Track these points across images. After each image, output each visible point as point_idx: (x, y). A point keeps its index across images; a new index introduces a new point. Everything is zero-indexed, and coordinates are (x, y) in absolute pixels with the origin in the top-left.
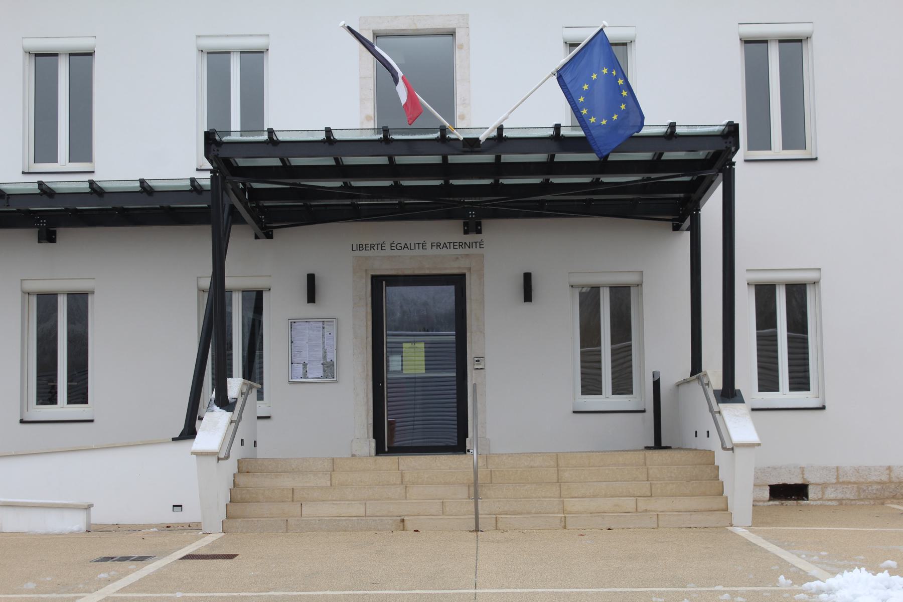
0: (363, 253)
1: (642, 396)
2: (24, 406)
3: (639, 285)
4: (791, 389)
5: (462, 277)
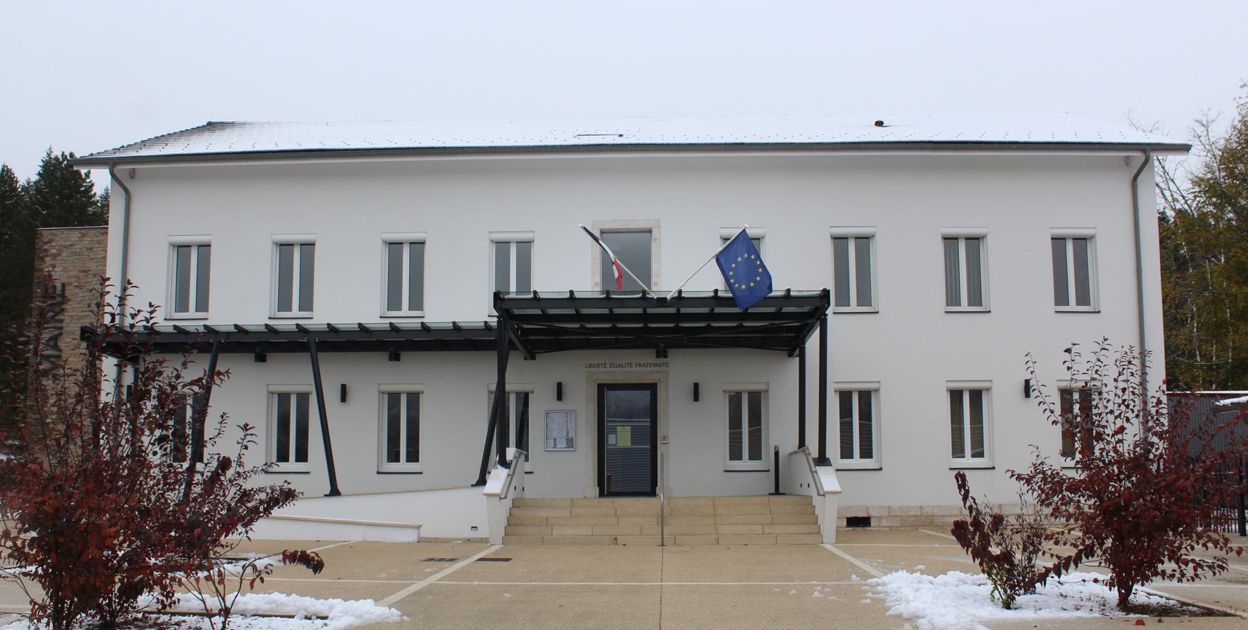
1: (767, 461)
3: (766, 391)
5: (655, 385)
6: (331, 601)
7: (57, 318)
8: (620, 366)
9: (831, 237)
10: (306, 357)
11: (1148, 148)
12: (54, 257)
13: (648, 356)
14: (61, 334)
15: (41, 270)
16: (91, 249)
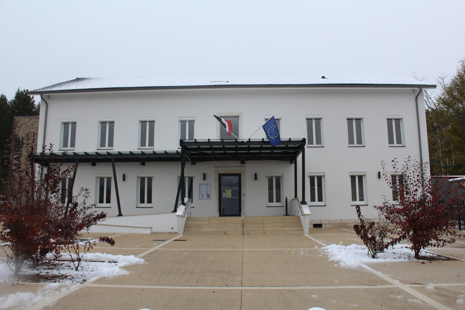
1: (283, 203)
2: (137, 204)
3: (282, 176)
6: (118, 256)
7: (20, 150)
11: (421, 86)
12: (20, 127)
13: (238, 163)
14: (21, 156)
15: (14, 132)
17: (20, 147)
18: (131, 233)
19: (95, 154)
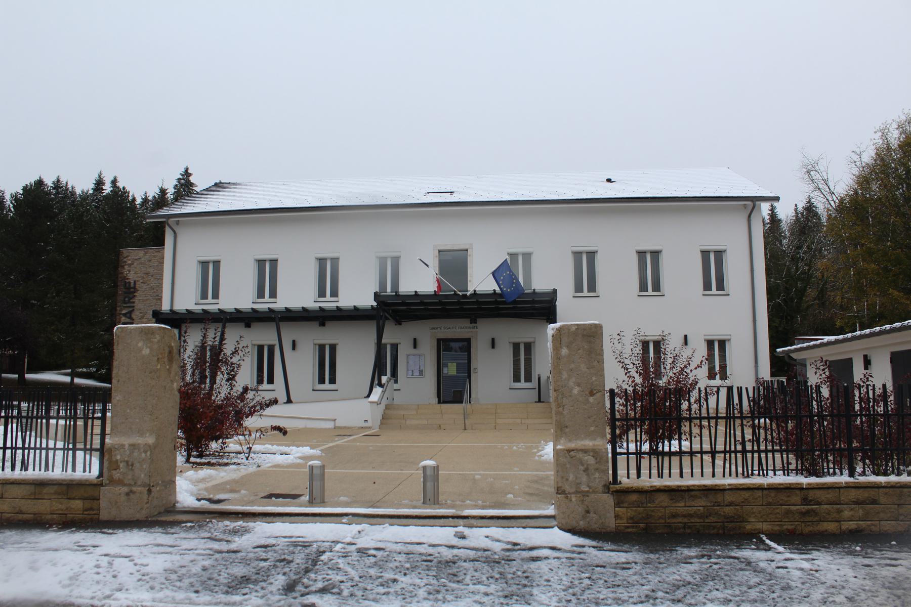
0: (434, 330)
1: (534, 384)
2: (314, 385)
3: (534, 342)
4: (525, 382)
5: (470, 339)
6: (291, 447)
7: (131, 301)
8: (449, 328)
9: (572, 252)
10: (274, 324)
11: (754, 199)
12: (130, 265)
13: (465, 323)
14: (133, 310)
15: (122, 273)
16: (150, 260)
17: (131, 296)
18: (306, 428)
19: (250, 311)
